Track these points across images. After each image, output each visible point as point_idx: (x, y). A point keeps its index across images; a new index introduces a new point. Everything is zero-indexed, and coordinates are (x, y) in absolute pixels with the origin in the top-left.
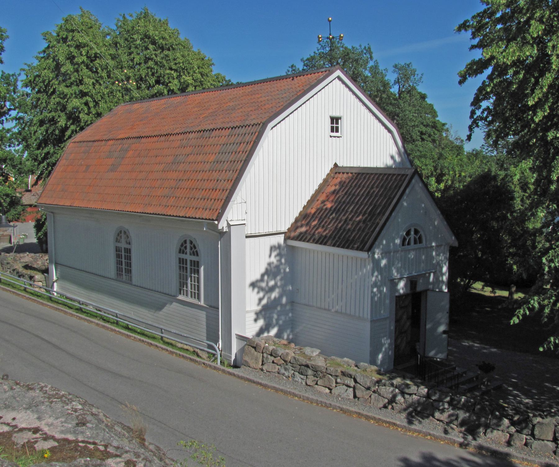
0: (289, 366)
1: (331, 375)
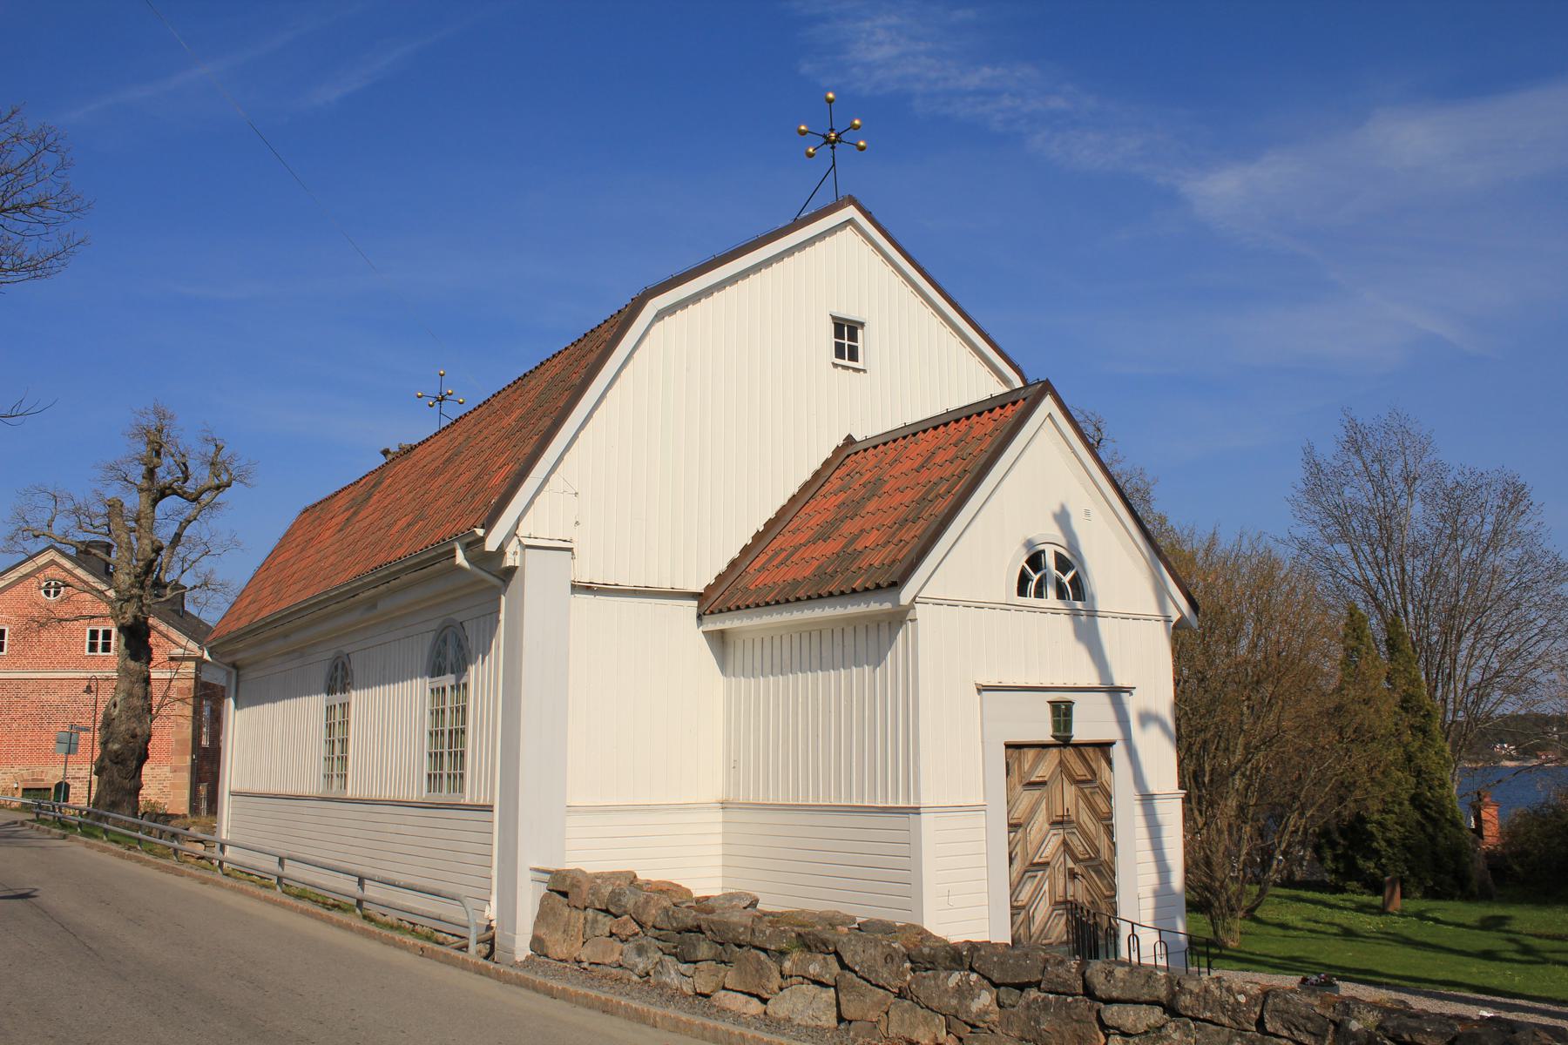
0: (649, 941)
1: (765, 950)
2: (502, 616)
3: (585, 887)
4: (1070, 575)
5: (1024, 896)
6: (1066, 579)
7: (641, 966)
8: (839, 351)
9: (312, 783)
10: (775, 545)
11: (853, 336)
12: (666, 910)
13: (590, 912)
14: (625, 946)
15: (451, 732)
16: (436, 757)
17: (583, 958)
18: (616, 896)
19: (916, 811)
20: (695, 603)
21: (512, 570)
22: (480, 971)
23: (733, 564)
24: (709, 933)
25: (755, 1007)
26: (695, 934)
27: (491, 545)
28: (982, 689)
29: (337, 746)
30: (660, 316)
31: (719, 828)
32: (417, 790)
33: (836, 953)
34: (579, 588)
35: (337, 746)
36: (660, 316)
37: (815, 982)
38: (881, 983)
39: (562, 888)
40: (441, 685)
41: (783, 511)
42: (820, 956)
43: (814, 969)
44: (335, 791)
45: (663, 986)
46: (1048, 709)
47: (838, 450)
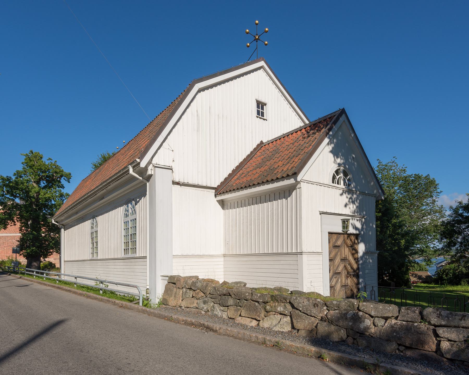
1: (258, 302)
2: (148, 193)
3: (182, 281)
7: (205, 308)
8: (258, 112)
9: (88, 256)
10: (241, 172)
12: (215, 288)
13: (184, 290)
14: (199, 301)
15: (131, 235)
16: (127, 243)
17: (182, 305)
18: (194, 283)
19: (301, 253)
20: (214, 191)
21: (151, 176)
22: (143, 312)
23: (226, 179)
24: (233, 296)
25: (254, 323)
26: (227, 295)
27: (143, 165)
28: (322, 213)
29: (95, 244)
30: (200, 91)
31: (222, 263)
32: (121, 254)
33: (290, 303)
34: (174, 183)
35: (95, 244)
36: (200, 91)
37: (281, 314)
38: (313, 315)
39: (173, 282)
40: (127, 220)
41: (241, 163)
42: (283, 304)
43: (280, 309)
44: (95, 257)
45: (216, 316)
46: (340, 223)
47: (258, 145)
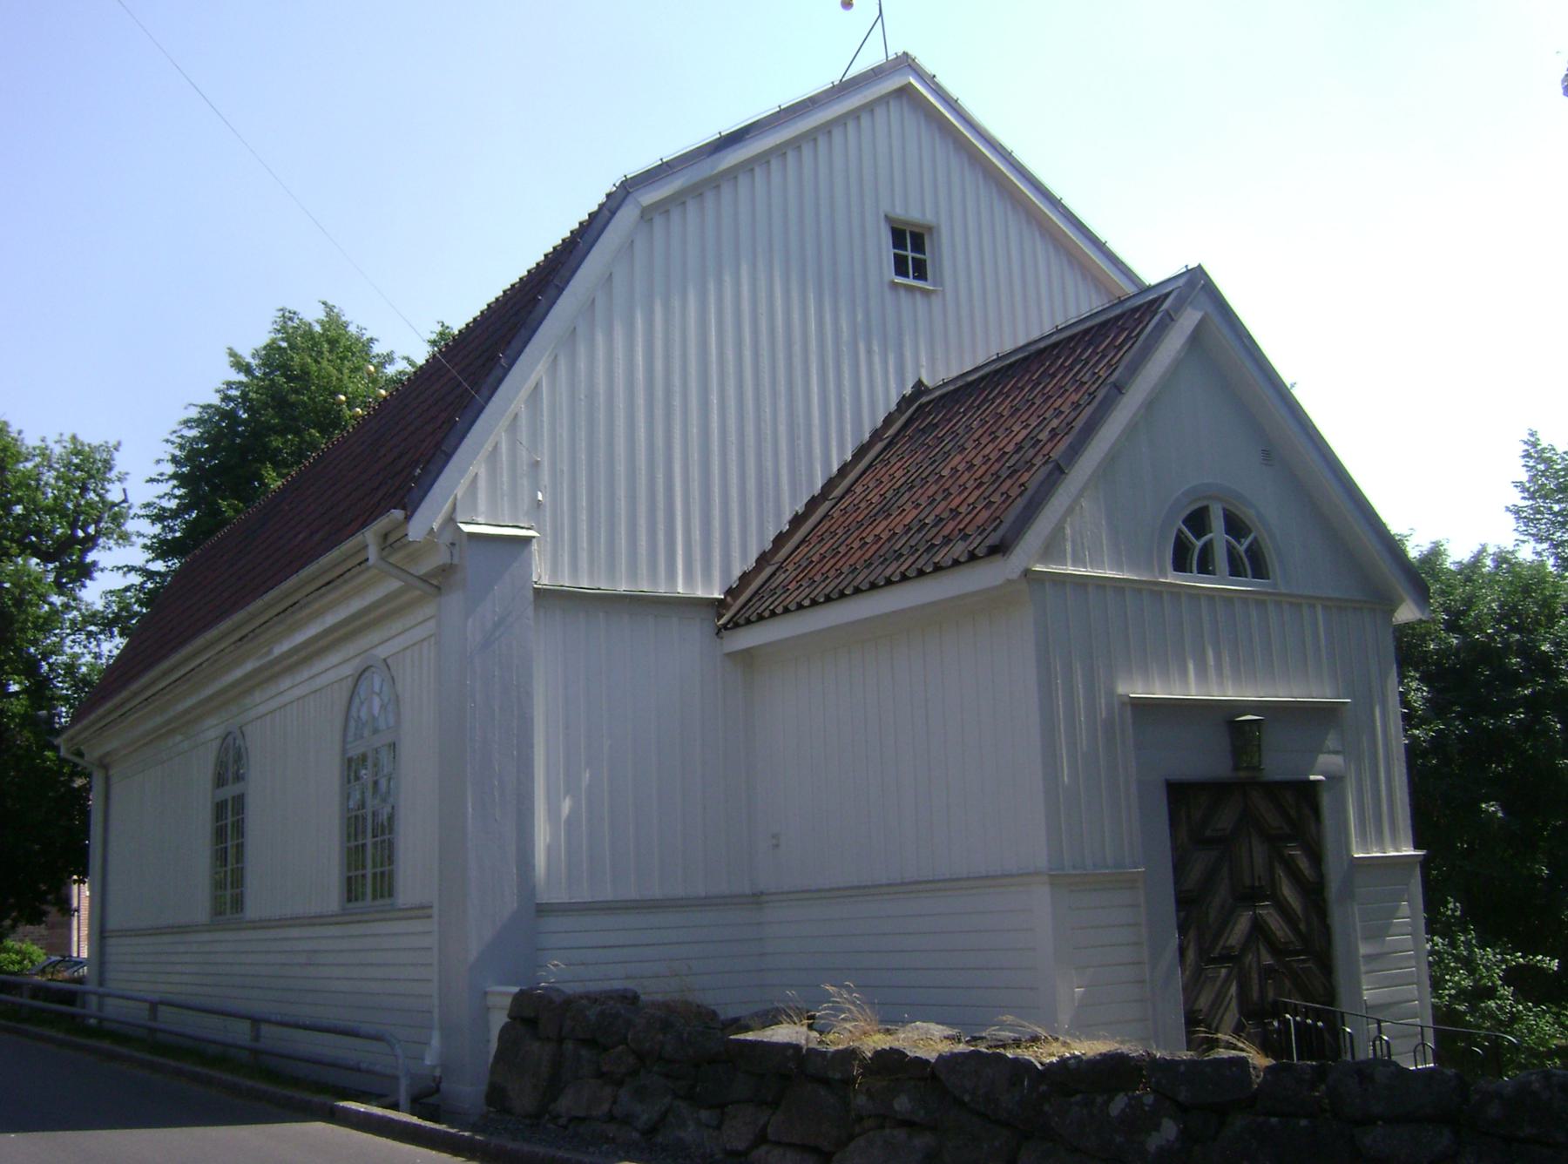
4: (1246, 542)
5: (1203, 1002)
6: (1242, 549)
8: (900, 267)
11: (918, 245)
15: (375, 875)
47: (905, 402)
